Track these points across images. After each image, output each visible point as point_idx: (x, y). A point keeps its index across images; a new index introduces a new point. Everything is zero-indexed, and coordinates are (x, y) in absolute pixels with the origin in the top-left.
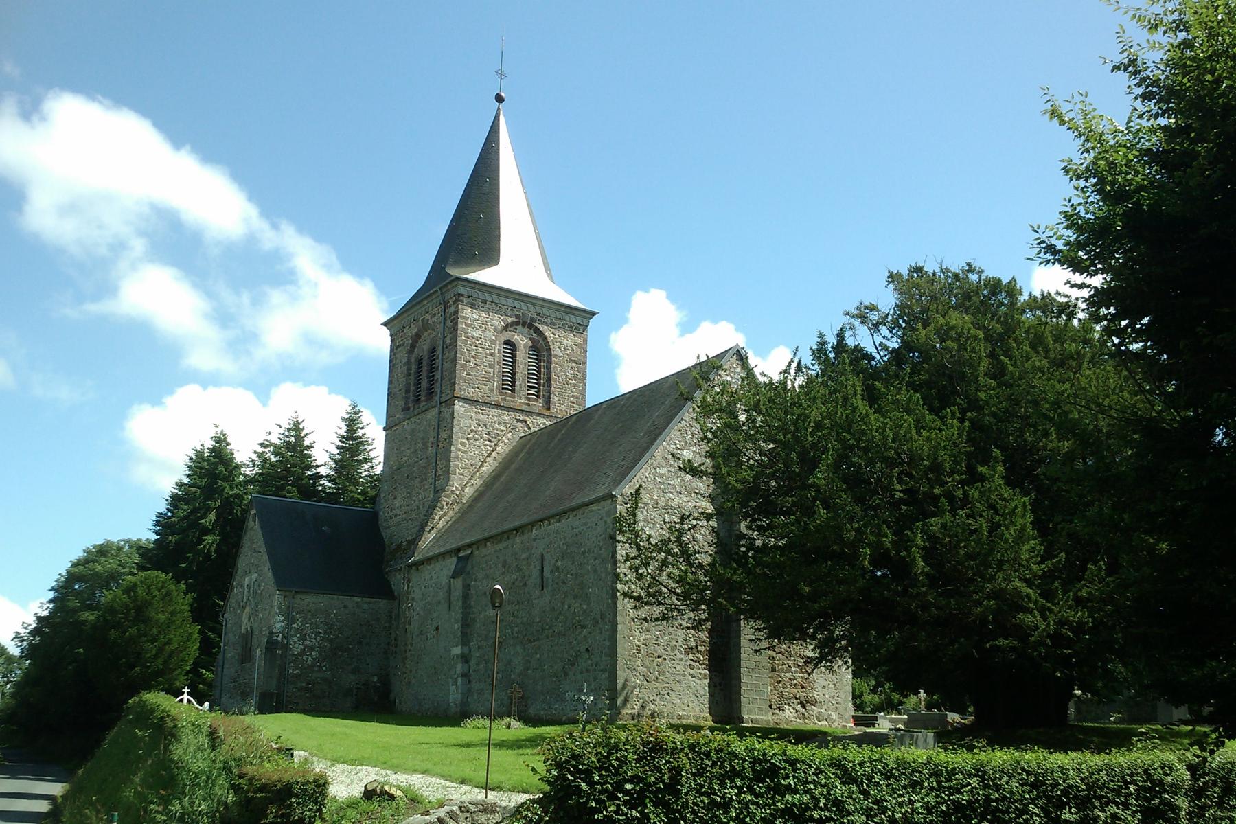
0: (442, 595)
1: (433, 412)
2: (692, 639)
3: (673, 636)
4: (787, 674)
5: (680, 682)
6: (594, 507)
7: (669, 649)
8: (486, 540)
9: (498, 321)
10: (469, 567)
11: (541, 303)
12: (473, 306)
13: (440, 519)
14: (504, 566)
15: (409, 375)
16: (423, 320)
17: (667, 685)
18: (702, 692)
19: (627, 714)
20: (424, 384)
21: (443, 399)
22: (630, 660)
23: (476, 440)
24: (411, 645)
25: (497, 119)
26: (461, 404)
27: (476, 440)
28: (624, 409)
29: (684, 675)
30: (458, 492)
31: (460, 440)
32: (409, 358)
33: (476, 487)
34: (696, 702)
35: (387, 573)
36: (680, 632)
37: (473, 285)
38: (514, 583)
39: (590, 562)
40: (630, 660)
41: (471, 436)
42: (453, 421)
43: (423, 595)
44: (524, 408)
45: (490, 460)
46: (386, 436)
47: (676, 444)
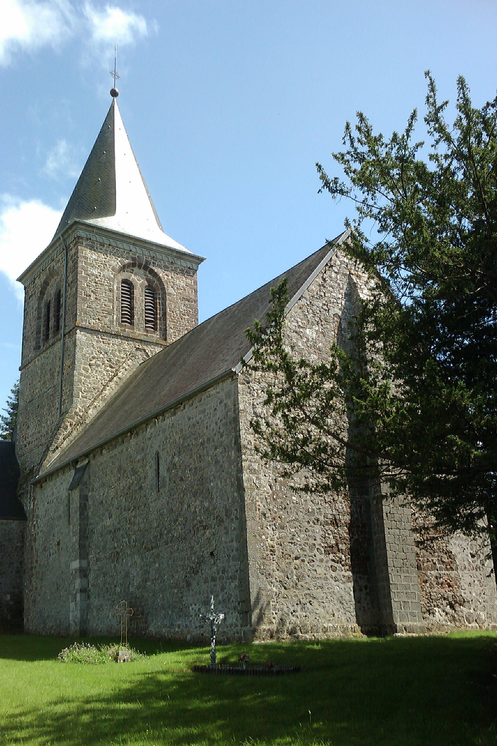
0: (62, 509)
1: (59, 344)
2: (331, 536)
3: (310, 533)
4: (432, 572)
5: (322, 588)
6: (212, 391)
7: (307, 548)
8: (101, 447)
9: (116, 262)
10: (86, 476)
11: (154, 248)
12: (92, 248)
13: (64, 439)
14: (119, 471)
15: (39, 318)
16: (49, 268)
17: (308, 592)
18: (347, 598)
19: (264, 630)
20: (52, 323)
21: (67, 330)
22: (264, 564)
23: (98, 366)
24: (37, 561)
25: (112, 108)
26: (82, 333)
27: (98, 366)
28: (236, 312)
29: (326, 579)
30: (81, 414)
31: (82, 366)
32: (39, 304)
33: (99, 409)
34: (342, 610)
35: (19, 496)
36: (318, 528)
37: (90, 229)
38: (129, 488)
39: (211, 453)
40: (264, 564)
41: (93, 362)
42: (75, 349)
43: (46, 511)
44: (142, 338)
45: (112, 384)
46: (21, 375)
47: (297, 322)
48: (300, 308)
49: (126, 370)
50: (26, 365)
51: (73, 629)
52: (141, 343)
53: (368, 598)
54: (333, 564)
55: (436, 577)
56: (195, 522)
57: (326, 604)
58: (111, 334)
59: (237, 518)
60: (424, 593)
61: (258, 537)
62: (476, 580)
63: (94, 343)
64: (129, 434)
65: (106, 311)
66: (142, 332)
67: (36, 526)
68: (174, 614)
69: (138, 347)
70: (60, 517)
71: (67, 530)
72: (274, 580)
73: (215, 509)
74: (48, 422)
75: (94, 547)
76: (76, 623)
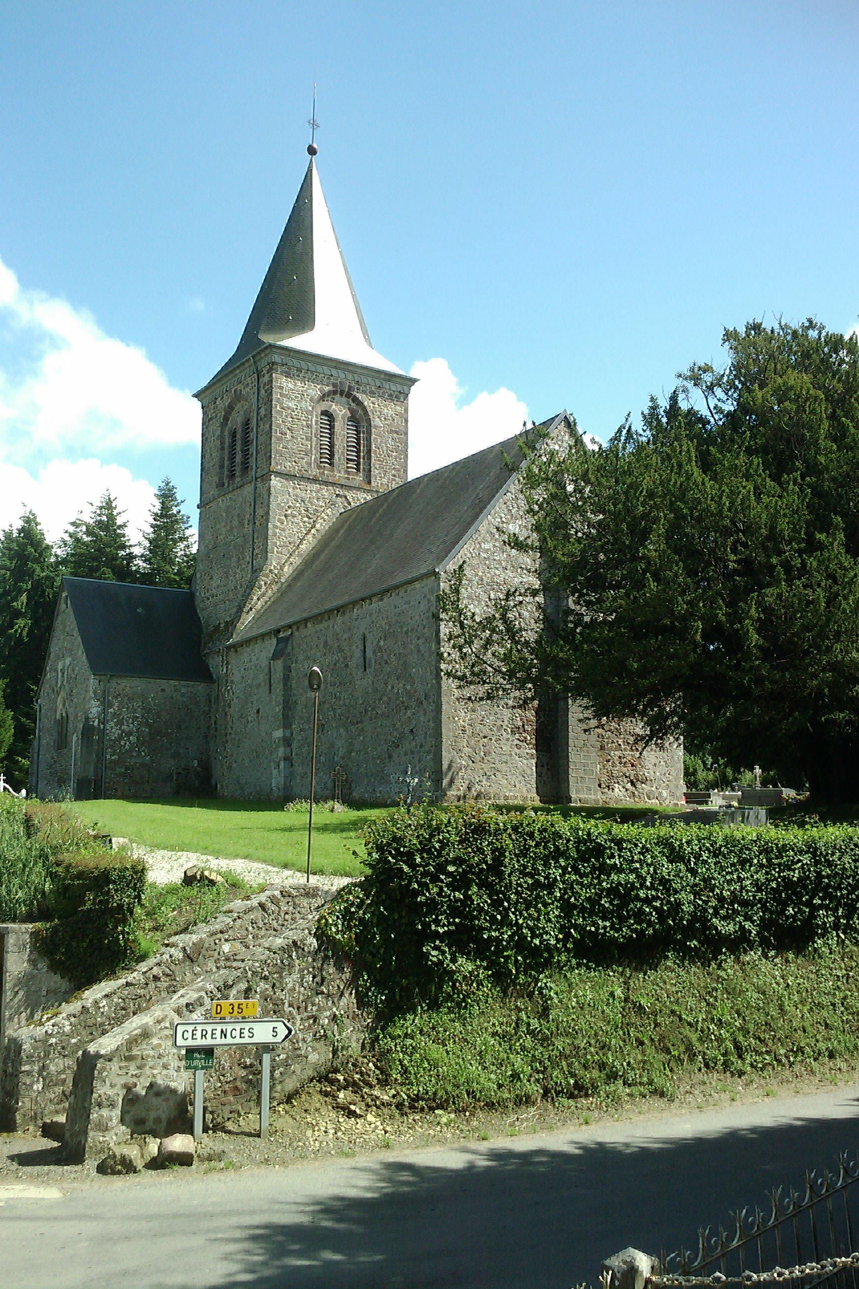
0: (262, 677)
1: (249, 488)
2: (518, 719)
3: (499, 716)
6: (417, 585)
7: (495, 729)
9: (315, 391)
10: (290, 647)
12: (288, 375)
13: (258, 599)
15: (223, 449)
17: (493, 765)
19: (453, 795)
20: (238, 459)
21: (259, 474)
23: (294, 516)
26: (277, 479)
27: (294, 516)
30: (276, 572)
31: (277, 517)
32: (222, 431)
33: (295, 566)
38: (335, 665)
39: (414, 642)
41: (289, 512)
42: (269, 497)
43: (243, 678)
44: (343, 482)
45: (310, 537)
46: (200, 514)
47: (501, 518)
48: (505, 503)
49: (324, 521)
50: (207, 504)
51: (276, 793)
52: (342, 488)
53: (549, 773)
54: (518, 742)
55: (620, 757)
56: (398, 702)
57: (509, 777)
58: (309, 479)
59: (434, 702)
60: (605, 771)
61: (451, 719)
62: (662, 761)
63: (290, 490)
64: (336, 612)
65: (302, 451)
66: (343, 474)
67: (231, 691)
68: (376, 782)
69: (338, 493)
70: (260, 685)
71: (268, 699)
72: (463, 755)
73: (415, 692)
74: (237, 576)
75: (297, 718)
76: (279, 789)
